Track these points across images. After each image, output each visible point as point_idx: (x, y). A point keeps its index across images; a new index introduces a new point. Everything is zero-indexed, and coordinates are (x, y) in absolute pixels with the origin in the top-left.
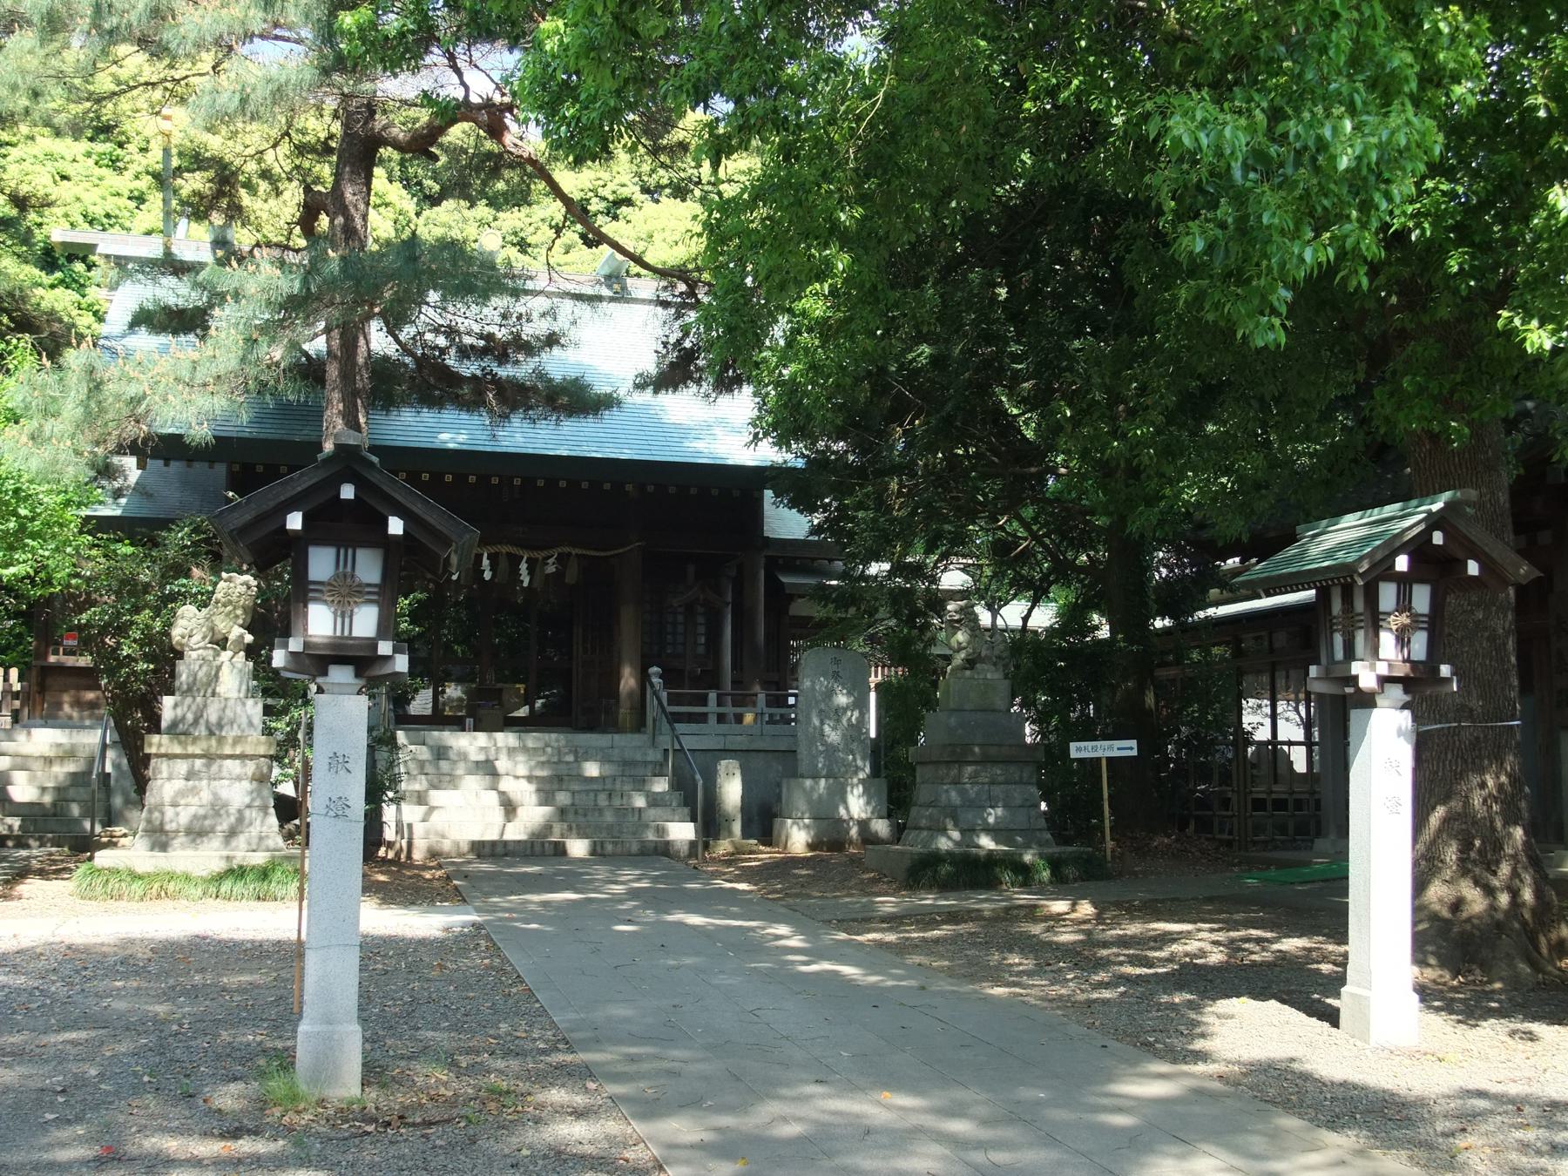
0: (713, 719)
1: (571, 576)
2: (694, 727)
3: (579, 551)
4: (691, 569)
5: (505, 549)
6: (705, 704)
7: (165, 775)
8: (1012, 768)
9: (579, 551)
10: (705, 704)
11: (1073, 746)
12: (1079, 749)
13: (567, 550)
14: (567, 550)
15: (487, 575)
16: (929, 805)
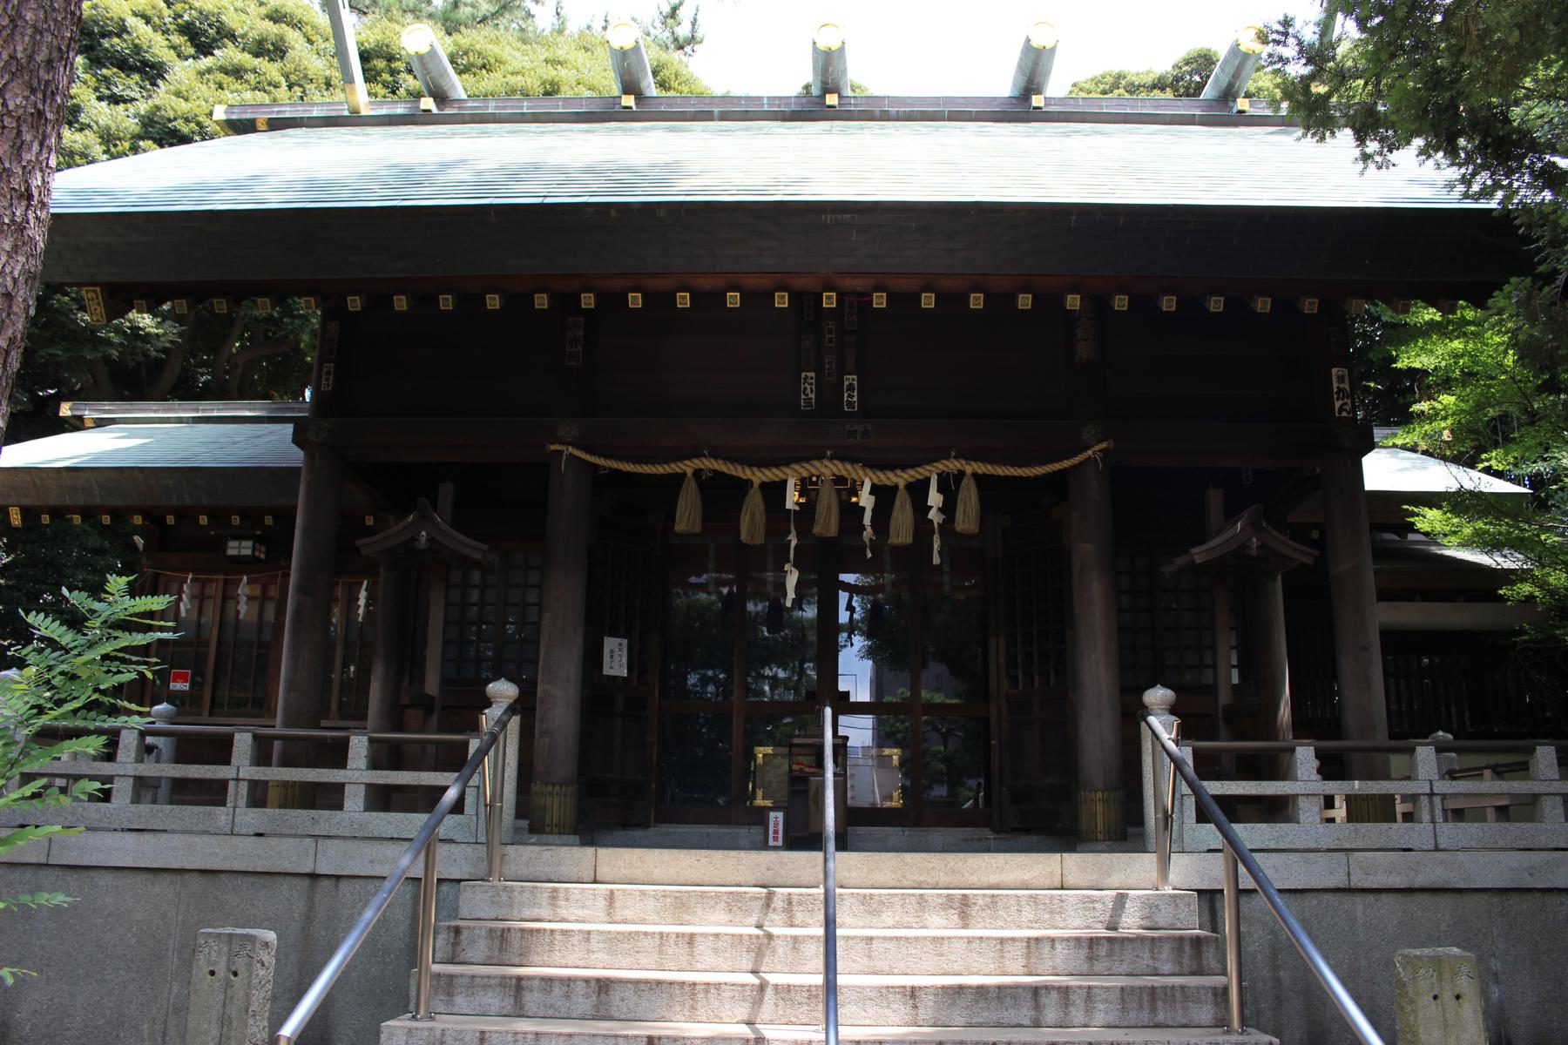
0: (354, 800)
1: (968, 518)
3: (981, 468)
5: (828, 469)
9: (981, 468)
11: (232, 544)
13: (952, 465)
14: (952, 465)
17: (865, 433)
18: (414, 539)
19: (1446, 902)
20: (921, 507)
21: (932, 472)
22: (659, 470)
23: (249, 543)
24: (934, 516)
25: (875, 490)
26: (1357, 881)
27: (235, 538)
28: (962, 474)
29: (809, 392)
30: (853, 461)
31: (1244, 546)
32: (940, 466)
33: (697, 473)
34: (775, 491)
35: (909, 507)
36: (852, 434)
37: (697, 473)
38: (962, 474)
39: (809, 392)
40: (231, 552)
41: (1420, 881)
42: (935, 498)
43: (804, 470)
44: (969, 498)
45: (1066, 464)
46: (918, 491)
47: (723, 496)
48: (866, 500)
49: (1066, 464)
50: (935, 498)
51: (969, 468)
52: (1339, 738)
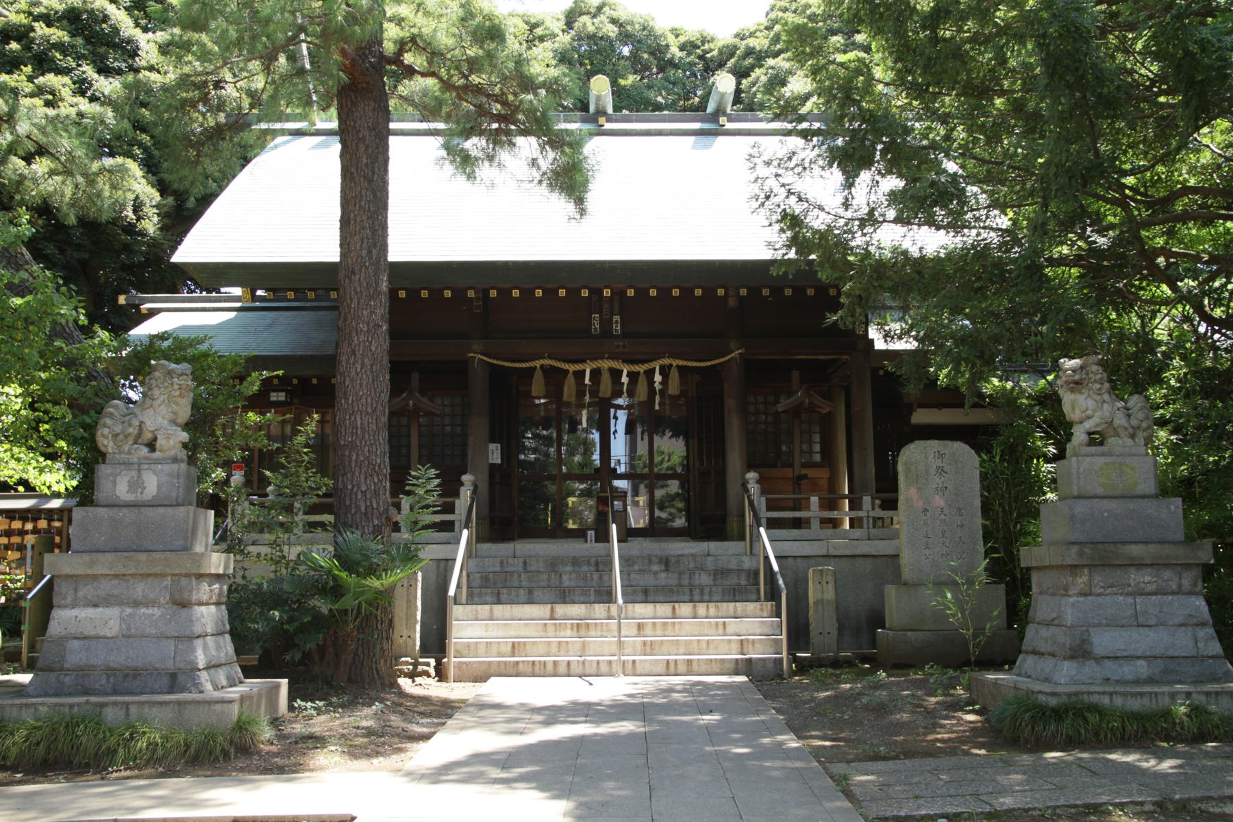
0: (815, 524)
1: (674, 388)
2: (795, 533)
3: (681, 363)
4: (795, 375)
5: (606, 364)
6: (808, 508)
7: (69, 600)
8: (1167, 574)
9: (681, 363)
10: (808, 508)
11: (272, 394)
12: (251, 660)
13: (667, 361)
14: (667, 361)
15: (657, 407)
16: (1049, 624)
17: (624, 346)
18: (407, 405)
19: (869, 561)
20: (651, 382)
21: (656, 365)
22: (524, 365)
23: (283, 394)
24: (657, 386)
25: (629, 374)
26: (832, 552)
27: (275, 391)
28: (671, 365)
29: (596, 325)
30: (617, 359)
31: (802, 403)
32: (661, 362)
33: (542, 366)
34: (580, 375)
35: (645, 383)
36: (618, 346)
37: (542, 366)
38: (671, 365)
39: (596, 325)
40: (273, 399)
41: (858, 552)
42: (658, 378)
43: (595, 365)
44: (674, 376)
45: (722, 360)
46: (650, 373)
47: (554, 378)
48: (625, 379)
49: (722, 360)
50: (658, 378)
51: (675, 363)
52: (619, 541)
